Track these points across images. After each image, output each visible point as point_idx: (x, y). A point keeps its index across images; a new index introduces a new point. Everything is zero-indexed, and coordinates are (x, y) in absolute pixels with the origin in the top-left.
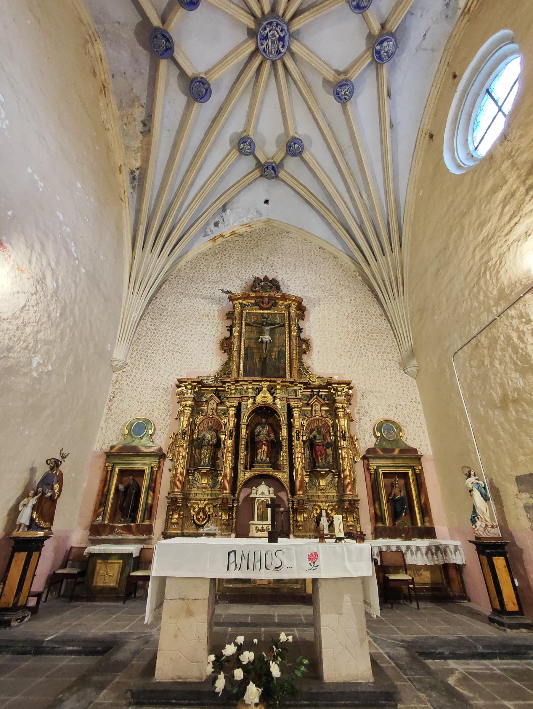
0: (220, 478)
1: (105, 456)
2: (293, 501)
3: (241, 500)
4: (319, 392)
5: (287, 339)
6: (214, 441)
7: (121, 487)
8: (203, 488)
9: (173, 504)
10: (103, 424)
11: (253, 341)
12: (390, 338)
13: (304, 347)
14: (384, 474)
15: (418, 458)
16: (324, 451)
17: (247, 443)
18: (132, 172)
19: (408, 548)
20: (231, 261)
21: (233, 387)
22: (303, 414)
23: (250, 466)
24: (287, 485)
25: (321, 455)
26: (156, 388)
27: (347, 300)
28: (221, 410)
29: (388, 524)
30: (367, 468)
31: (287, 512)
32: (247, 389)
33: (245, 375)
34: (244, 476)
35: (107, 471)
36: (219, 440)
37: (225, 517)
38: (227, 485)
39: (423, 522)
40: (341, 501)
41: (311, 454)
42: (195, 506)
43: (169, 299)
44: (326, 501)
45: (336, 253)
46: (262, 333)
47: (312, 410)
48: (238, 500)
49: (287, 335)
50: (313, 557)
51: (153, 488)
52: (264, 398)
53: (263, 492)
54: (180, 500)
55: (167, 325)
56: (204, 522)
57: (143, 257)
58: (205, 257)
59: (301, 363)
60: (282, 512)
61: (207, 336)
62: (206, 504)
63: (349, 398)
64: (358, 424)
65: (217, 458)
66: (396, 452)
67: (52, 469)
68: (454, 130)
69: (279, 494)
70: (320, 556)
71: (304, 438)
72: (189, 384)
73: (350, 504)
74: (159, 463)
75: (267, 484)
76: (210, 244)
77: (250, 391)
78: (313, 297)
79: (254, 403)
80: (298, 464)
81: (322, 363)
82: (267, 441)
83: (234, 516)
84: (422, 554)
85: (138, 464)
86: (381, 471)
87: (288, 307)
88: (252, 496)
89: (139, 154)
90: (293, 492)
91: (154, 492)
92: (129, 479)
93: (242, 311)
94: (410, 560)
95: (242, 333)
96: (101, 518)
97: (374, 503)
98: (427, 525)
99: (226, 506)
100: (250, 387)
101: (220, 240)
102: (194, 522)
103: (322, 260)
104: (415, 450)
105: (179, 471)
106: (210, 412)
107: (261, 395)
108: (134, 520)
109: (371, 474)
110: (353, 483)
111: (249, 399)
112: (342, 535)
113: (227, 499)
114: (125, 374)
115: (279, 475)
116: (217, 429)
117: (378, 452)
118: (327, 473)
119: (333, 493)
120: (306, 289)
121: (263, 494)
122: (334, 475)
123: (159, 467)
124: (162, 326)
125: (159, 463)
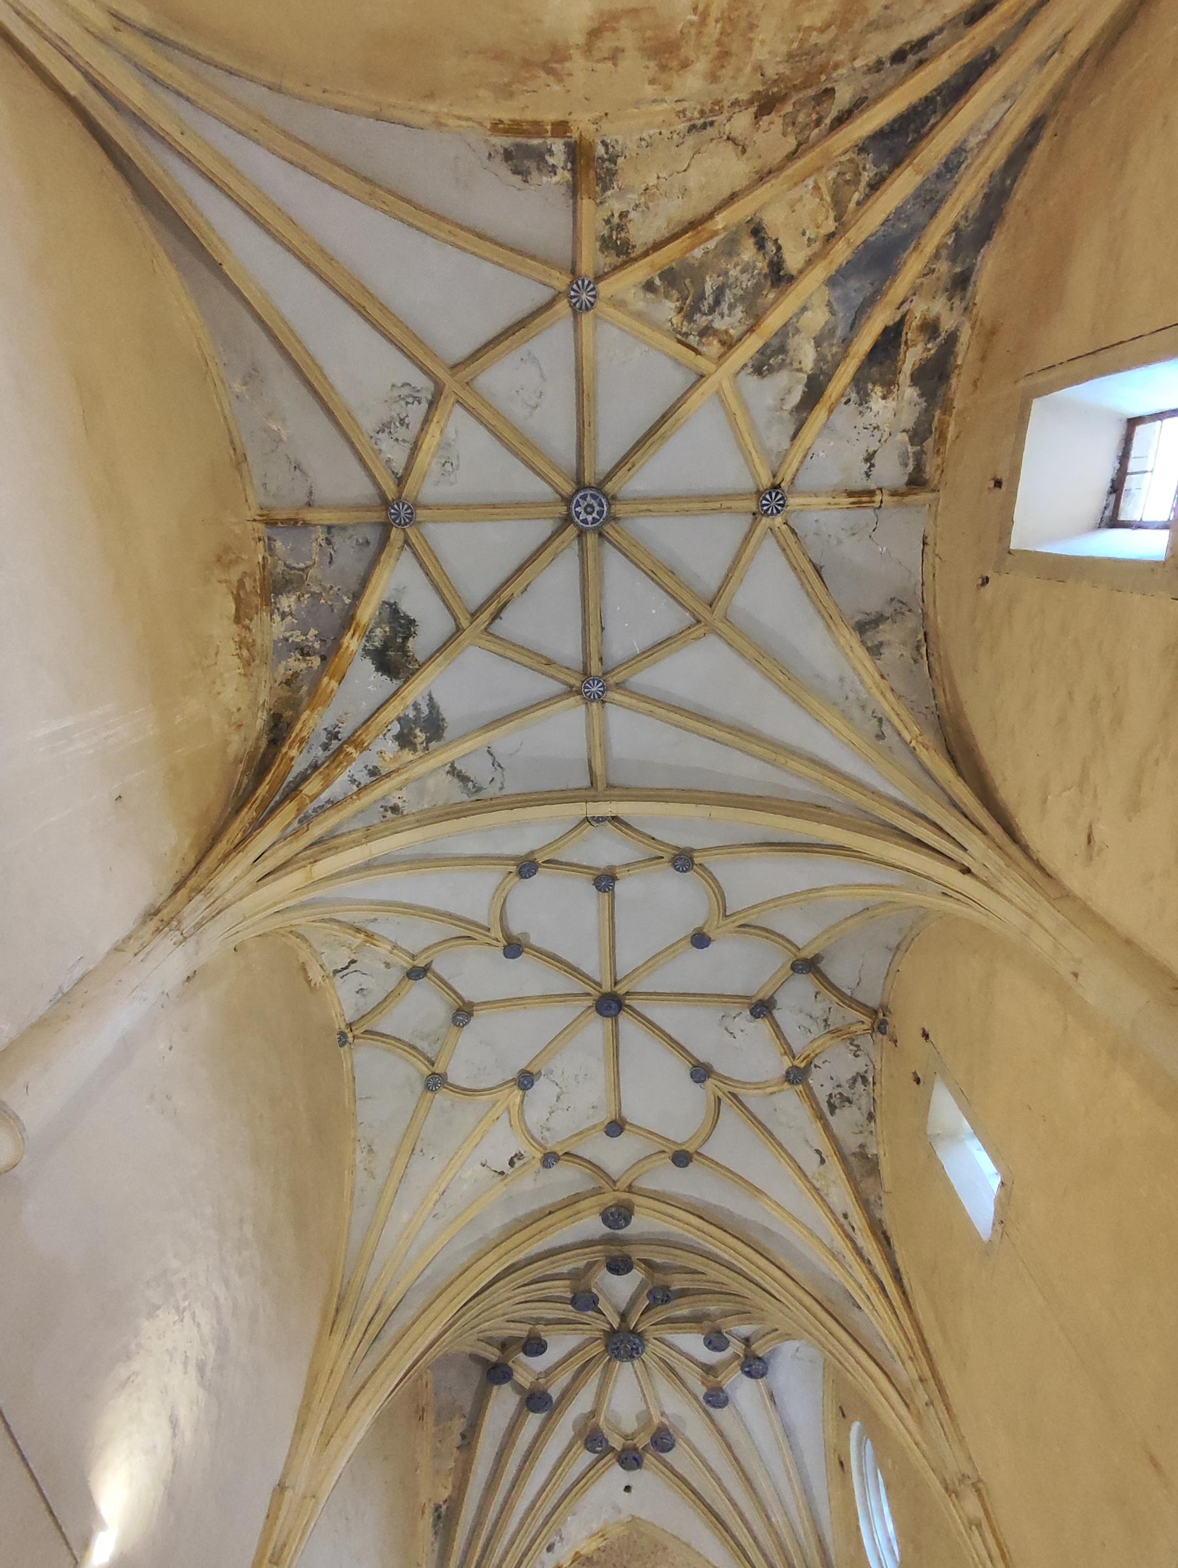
18: (437, 1508)
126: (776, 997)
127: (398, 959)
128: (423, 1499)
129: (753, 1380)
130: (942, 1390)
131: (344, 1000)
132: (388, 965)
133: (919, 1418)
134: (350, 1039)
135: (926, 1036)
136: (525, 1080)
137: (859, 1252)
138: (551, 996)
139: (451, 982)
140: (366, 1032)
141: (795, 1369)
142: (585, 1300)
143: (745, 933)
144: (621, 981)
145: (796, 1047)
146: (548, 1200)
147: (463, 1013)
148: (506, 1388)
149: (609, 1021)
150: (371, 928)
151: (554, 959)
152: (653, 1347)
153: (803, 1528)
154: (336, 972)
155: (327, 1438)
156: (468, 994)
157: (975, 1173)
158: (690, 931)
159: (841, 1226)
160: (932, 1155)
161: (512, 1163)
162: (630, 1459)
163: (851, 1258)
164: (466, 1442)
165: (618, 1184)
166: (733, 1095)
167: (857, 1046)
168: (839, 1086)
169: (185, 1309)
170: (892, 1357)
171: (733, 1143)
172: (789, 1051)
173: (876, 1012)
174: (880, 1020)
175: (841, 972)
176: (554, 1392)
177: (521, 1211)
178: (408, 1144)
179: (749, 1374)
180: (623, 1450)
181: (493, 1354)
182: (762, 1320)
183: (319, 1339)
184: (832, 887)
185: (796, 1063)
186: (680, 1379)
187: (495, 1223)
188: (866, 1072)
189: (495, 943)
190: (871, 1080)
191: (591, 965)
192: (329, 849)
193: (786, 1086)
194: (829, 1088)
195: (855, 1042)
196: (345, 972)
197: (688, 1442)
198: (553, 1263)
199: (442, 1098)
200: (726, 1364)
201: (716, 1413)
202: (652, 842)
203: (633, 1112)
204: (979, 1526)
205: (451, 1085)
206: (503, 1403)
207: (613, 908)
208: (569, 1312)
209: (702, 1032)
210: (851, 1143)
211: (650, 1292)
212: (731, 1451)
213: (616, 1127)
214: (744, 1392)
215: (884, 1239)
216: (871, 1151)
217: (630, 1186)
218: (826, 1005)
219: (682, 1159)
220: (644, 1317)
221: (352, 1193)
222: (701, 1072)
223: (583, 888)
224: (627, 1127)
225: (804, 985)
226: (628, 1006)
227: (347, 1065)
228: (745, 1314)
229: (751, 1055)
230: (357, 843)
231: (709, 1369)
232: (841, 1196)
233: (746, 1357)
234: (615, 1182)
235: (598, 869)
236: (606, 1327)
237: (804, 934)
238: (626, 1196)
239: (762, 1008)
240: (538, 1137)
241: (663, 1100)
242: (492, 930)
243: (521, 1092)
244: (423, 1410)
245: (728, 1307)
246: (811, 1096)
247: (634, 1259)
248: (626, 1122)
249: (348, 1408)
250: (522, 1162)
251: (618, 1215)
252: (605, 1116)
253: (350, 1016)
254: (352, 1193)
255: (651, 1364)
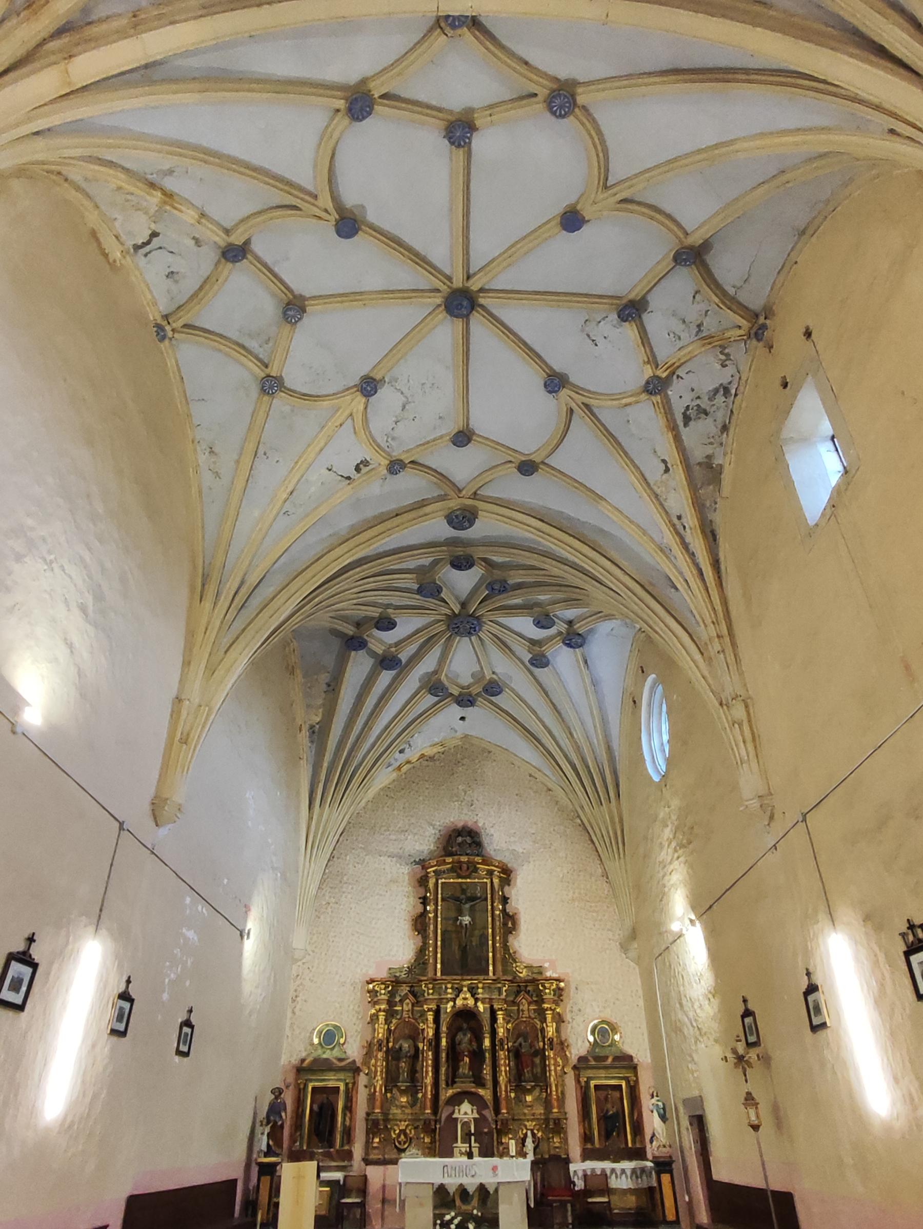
0: (420, 1095)
1: (295, 1070)
2: (496, 1121)
3: (443, 1119)
4: (526, 986)
5: (490, 919)
6: (412, 1052)
7: (315, 1107)
8: (403, 1107)
9: (374, 1127)
10: (288, 1032)
11: (451, 922)
12: (611, 909)
13: (510, 925)
14: (595, 1086)
15: (634, 1068)
16: (530, 1059)
17: (447, 1055)
18: (312, 727)
19: (613, 1170)
20: (421, 798)
21: (431, 986)
22: (508, 1016)
23: (451, 1083)
24: (490, 1104)
25: (527, 1066)
26: (343, 984)
27: (562, 854)
28: (418, 1011)
29: (597, 1145)
30: (578, 1081)
31: (490, 1133)
32: (446, 988)
33: (442, 974)
34: (447, 1093)
35: (300, 1090)
36: (417, 1049)
37: (427, 1140)
38: (428, 1104)
39: (634, 1142)
40: (547, 1121)
41: (517, 1065)
42: (396, 1128)
43: (348, 858)
44: (532, 1120)
45: (550, 785)
46: (460, 912)
47: (518, 1010)
48: (440, 1121)
49: (489, 915)
50: (495, 1169)
51: (349, 1107)
52: (465, 1000)
53: (466, 1112)
54: (381, 1122)
55: (349, 896)
56: (406, 1146)
57: (321, 815)
58: (389, 794)
59: (506, 947)
60: (486, 1133)
61: (397, 911)
62: (407, 1126)
63: (559, 992)
64: (570, 1026)
65: (416, 1072)
66: (610, 1060)
67: (276, 1098)
68: (649, 714)
69: (484, 1112)
70: (499, 1168)
71: (510, 1044)
72: (382, 984)
73: (555, 1123)
74: (354, 1078)
75: (469, 1102)
76: (394, 775)
77: (450, 991)
78: (521, 850)
79: (454, 1007)
80: (502, 1079)
81: (532, 947)
82: (469, 1051)
83: (437, 1137)
84: (627, 1177)
85: (332, 1080)
86: (593, 1083)
87: (490, 873)
88: (455, 1116)
89: (321, 710)
90: (497, 1111)
91: (351, 1112)
92: (322, 1098)
93: (437, 881)
94: (614, 1183)
95: (437, 911)
96: (298, 1144)
97: (584, 1121)
98: (638, 1146)
99: (428, 1128)
100: (449, 986)
101: (404, 769)
102: (396, 1146)
103: (532, 794)
104: (631, 1058)
105: (378, 1089)
106: (405, 1015)
107: (462, 995)
108: (331, 1145)
109: (581, 1087)
110: (562, 1100)
111: (448, 1002)
112: (514, 1154)
113: (430, 1120)
114: (306, 966)
115: (481, 1092)
116: (415, 1035)
117: (589, 1061)
118: (533, 1088)
119: (539, 1110)
120: (512, 839)
121: (466, 1113)
122: (541, 1090)
123: (354, 1084)
124: (343, 899)
125: (354, 1078)
126: (649, 298)
127: (209, 233)
128: (299, 721)
129: (572, 650)
130: (734, 645)
131: (154, 285)
132: (198, 242)
133: (709, 661)
134: (170, 334)
135: (808, 334)
136: (369, 386)
137: (685, 546)
138: (392, 292)
139: (276, 269)
140: (186, 326)
141: (609, 648)
142: (429, 589)
143: (627, 210)
144: (475, 274)
145: (661, 357)
146: (391, 506)
147: (294, 308)
148: (362, 653)
149: (459, 323)
150: (169, 183)
151: (396, 243)
152: (488, 627)
153: (598, 740)
154: (137, 248)
155: (211, 670)
156: (299, 286)
157: (817, 470)
158: (560, 209)
159: (674, 526)
160: (780, 461)
161: (358, 469)
162: (466, 700)
163: (677, 551)
164: (331, 688)
165: (464, 492)
166: (587, 406)
167: (728, 355)
168: (699, 398)
169: (51, 562)
170: (698, 623)
171: (581, 454)
172: (652, 360)
173: (757, 316)
174: (759, 326)
175: (728, 267)
176: (404, 657)
177: (369, 513)
178: (251, 447)
179: (569, 645)
180: (459, 695)
181: (350, 630)
182: (587, 605)
183: (190, 608)
184: (744, 139)
185: (659, 373)
186: (510, 650)
187: (345, 523)
188: (730, 383)
189: (323, 215)
190: (733, 391)
191: (440, 251)
192: (87, 41)
193: (644, 396)
194: (686, 401)
195: (726, 351)
196: (148, 248)
197: (513, 690)
198: (401, 558)
199: (281, 402)
200: (551, 638)
201: (537, 671)
202: (522, 69)
203: (481, 423)
204: (740, 725)
205: (289, 390)
206: (359, 665)
207: (469, 174)
208: (417, 600)
209: (559, 336)
210: (698, 454)
211: (489, 584)
212: (547, 696)
213: (463, 438)
214: (563, 659)
215: (711, 535)
216: (717, 461)
217: (475, 493)
218: (703, 307)
219: (527, 468)
220: (483, 604)
221: (200, 492)
222: (555, 382)
223: (430, 140)
224: (474, 438)
225: (685, 281)
226: (482, 306)
227: (171, 363)
228: (571, 602)
229: (611, 362)
230: (121, 34)
231: (533, 642)
232: (679, 500)
233: (568, 634)
234: (460, 491)
235: (451, 112)
236: (448, 612)
237: (696, 212)
238: (470, 502)
239: (632, 310)
240: (384, 445)
241: (512, 409)
242: (320, 197)
243: (364, 400)
244: (293, 667)
245: (560, 596)
246: (667, 409)
247: (475, 558)
248: (474, 433)
249: (226, 652)
250: (368, 469)
251: (463, 518)
252: (451, 427)
253: (164, 306)
254: (200, 492)
255: (487, 641)
